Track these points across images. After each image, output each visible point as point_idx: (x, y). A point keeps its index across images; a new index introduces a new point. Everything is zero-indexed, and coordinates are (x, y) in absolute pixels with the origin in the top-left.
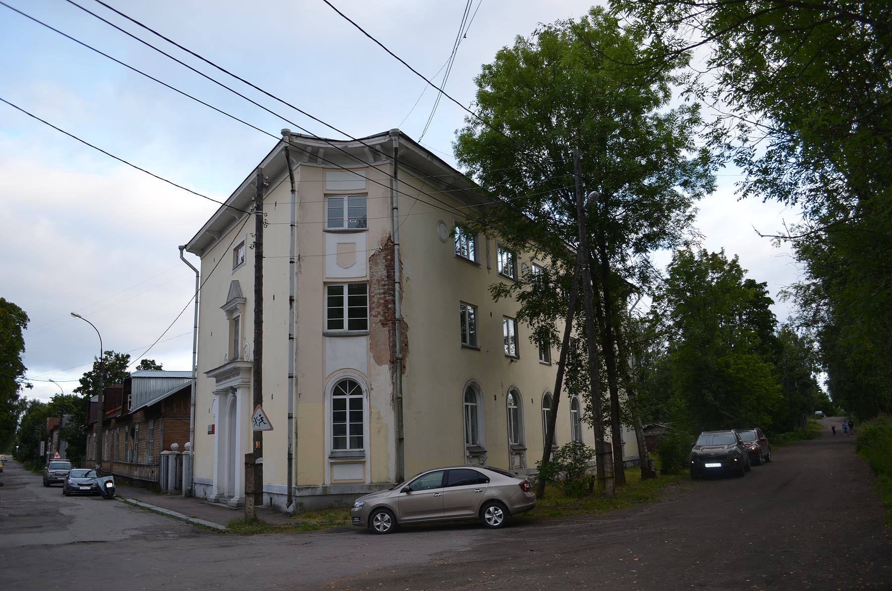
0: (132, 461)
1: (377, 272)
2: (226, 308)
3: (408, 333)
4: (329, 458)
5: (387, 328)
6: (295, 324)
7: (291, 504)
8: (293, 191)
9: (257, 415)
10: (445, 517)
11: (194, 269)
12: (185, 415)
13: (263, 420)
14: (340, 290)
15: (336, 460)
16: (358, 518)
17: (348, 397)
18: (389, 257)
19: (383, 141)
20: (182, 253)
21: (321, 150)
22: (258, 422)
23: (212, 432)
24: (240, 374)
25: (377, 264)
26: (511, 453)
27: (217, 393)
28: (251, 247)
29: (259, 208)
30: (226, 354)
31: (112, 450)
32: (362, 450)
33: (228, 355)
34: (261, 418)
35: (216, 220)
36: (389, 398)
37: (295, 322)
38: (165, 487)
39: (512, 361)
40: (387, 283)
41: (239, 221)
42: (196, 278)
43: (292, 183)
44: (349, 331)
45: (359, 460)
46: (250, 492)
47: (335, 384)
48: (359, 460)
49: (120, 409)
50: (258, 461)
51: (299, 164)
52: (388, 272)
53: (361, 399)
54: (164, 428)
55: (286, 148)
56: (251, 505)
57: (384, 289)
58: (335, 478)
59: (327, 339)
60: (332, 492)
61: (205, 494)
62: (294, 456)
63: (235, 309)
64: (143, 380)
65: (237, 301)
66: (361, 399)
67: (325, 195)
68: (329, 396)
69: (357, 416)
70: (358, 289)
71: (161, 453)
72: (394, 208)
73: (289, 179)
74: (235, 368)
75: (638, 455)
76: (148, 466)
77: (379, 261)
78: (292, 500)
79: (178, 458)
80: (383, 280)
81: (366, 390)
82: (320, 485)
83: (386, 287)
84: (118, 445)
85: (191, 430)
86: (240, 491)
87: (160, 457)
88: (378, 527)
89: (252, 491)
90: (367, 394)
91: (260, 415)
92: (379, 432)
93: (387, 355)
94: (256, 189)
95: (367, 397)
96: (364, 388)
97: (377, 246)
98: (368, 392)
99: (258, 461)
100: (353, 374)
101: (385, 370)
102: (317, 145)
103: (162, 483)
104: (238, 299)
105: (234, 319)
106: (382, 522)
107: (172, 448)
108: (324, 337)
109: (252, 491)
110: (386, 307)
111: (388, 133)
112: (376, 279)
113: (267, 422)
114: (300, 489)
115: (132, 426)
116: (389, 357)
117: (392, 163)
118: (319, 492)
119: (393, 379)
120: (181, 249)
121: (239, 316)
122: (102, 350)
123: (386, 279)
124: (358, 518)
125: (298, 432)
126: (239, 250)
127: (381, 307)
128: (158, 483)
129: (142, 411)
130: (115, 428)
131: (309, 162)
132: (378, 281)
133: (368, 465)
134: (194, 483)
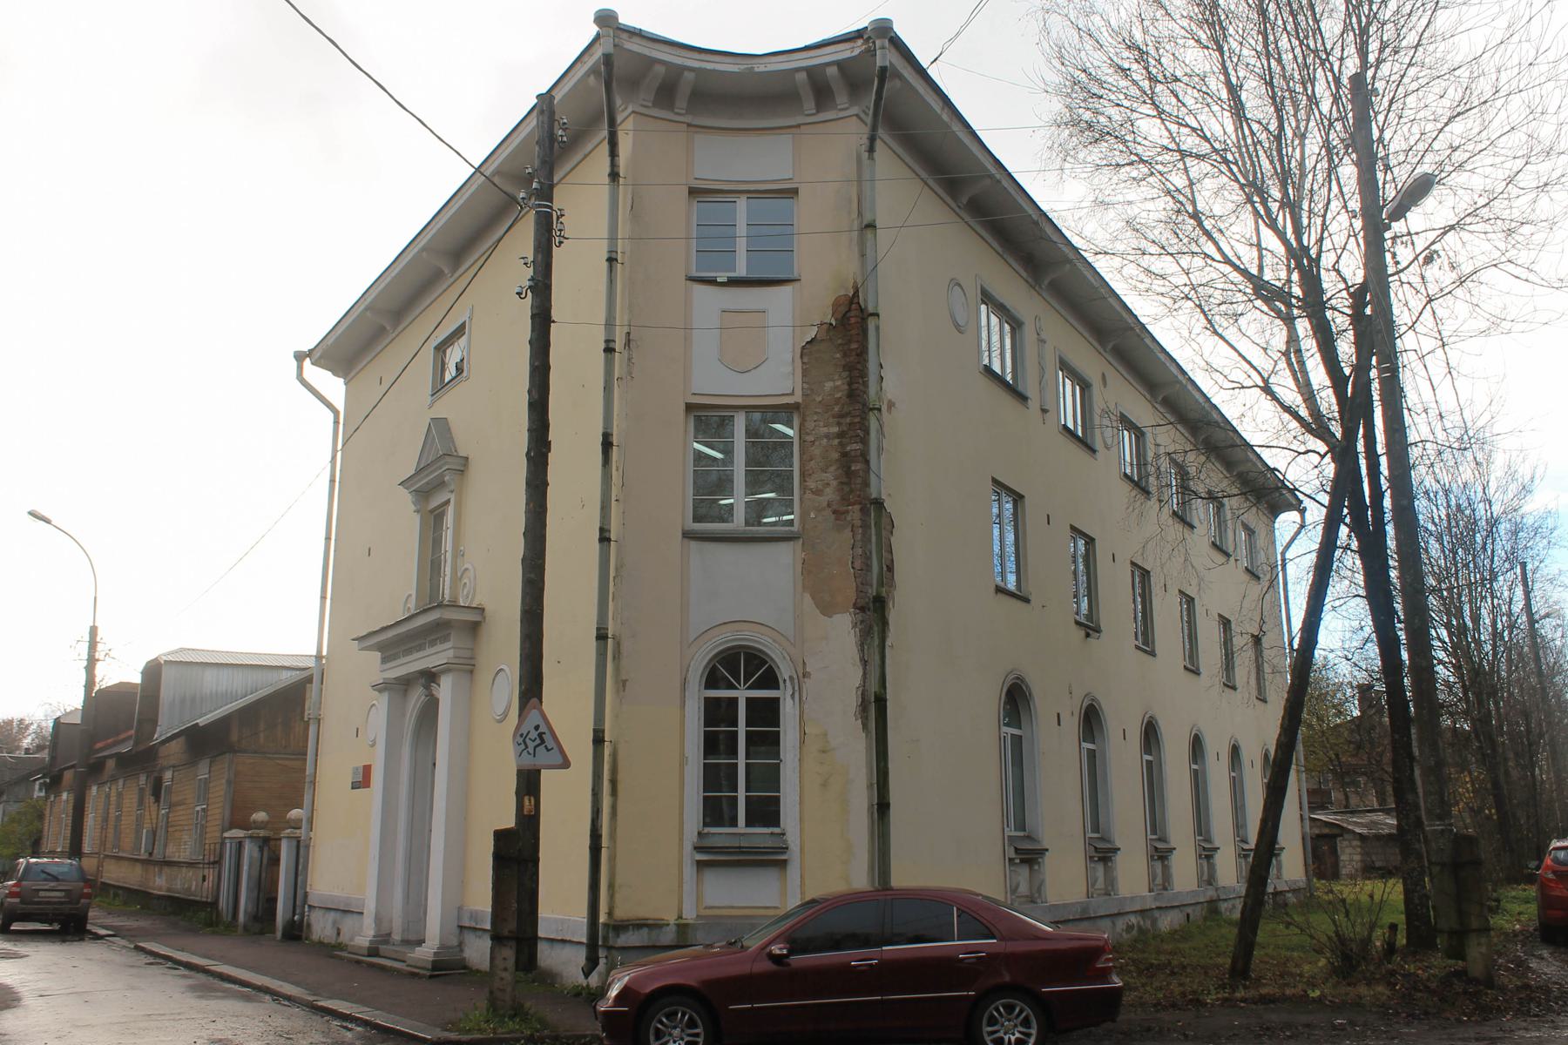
0: (151, 854)
2: (412, 485)
3: (892, 540)
4: (695, 848)
6: (613, 503)
7: (594, 969)
8: (614, 176)
9: (528, 726)
13: (543, 741)
15: (713, 859)
17: (742, 694)
18: (854, 346)
19: (847, 54)
20: (300, 368)
21: (686, 73)
22: (531, 745)
23: (363, 780)
26: (1090, 857)
27: (381, 688)
28: (519, 294)
29: (546, 193)
30: (410, 595)
31: (104, 829)
32: (776, 830)
33: (414, 596)
34: (540, 735)
36: (853, 701)
37: (613, 498)
39: (1088, 635)
41: (452, 280)
42: (332, 425)
43: (613, 153)
44: (747, 528)
45: (772, 859)
47: (711, 660)
48: (772, 859)
49: (129, 738)
51: (630, 110)
52: (850, 384)
53: (777, 700)
55: (607, 59)
56: (505, 969)
57: (839, 424)
58: (710, 902)
59: (694, 545)
61: (339, 934)
62: (605, 842)
63: (440, 484)
65: (446, 463)
66: (777, 700)
67: (693, 192)
68: (697, 689)
71: (226, 835)
73: (605, 147)
74: (438, 624)
75: (1304, 878)
76: (191, 865)
78: (598, 958)
79: (266, 849)
81: (791, 678)
82: (671, 918)
84: (118, 818)
85: (307, 780)
87: (223, 844)
89: (509, 932)
90: (793, 688)
91: (537, 728)
92: (824, 785)
93: (848, 591)
94: (537, 148)
95: (793, 696)
96: (784, 671)
98: (796, 681)
101: (842, 629)
102: (679, 61)
103: (224, 903)
104: (448, 459)
105: (432, 511)
107: (254, 822)
108: (686, 540)
109: (509, 932)
111: (859, 34)
112: (819, 399)
115: (156, 774)
116: (851, 594)
117: (862, 115)
120: (300, 357)
121: (448, 502)
125: (621, 776)
126: (448, 351)
128: (214, 904)
129: (182, 740)
130: (114, 779)
133: (793, 871)
134: (310, 906)
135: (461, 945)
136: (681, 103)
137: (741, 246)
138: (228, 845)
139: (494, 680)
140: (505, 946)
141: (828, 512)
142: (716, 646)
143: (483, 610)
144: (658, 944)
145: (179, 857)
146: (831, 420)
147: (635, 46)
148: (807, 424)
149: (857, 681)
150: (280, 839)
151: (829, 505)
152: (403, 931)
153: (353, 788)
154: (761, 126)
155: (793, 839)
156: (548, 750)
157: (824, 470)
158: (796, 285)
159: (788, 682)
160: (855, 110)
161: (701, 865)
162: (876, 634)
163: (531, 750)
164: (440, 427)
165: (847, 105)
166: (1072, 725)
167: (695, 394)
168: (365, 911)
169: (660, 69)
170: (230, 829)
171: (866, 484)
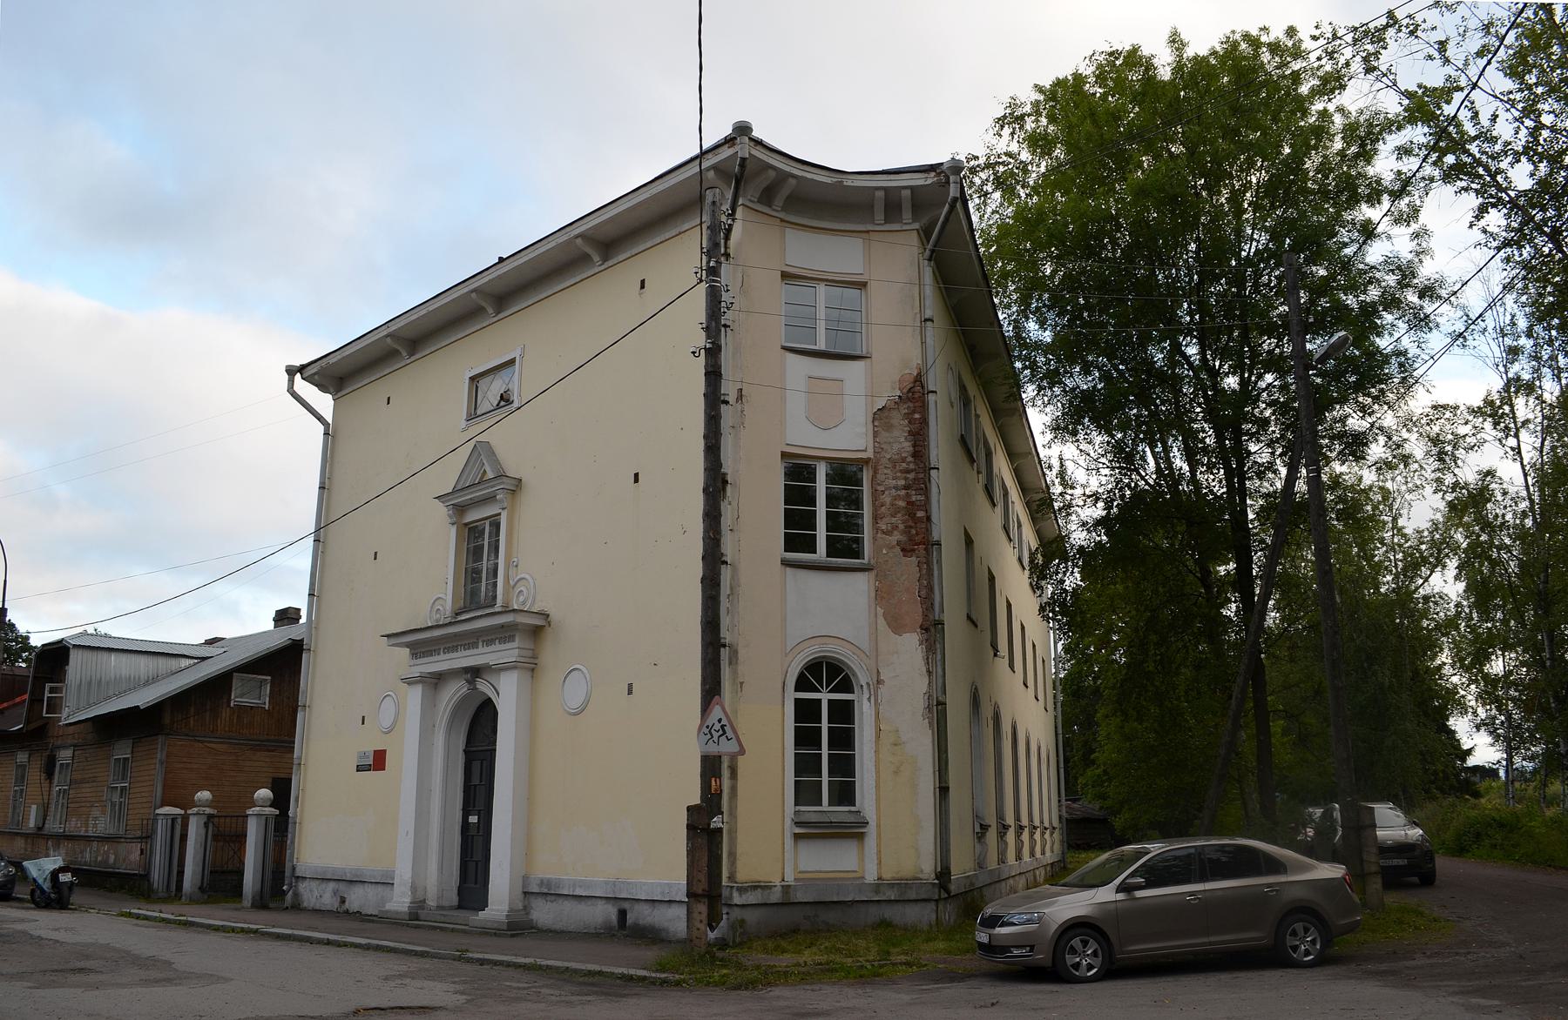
1: (890, 443)
5: (914, 558)
10: (1210, 943)
11: (320, 418)
12: (212, 732)
13: (724, 733)
14: (810, 474)
15: (810, 832)
16: (1028, 949)
18: (917, 416)
19: (921, 182)
20: (291, 382)
22: (716, 735)
24: (517, 639)
25: (889, 427)
28: (694, 353)
32: (853, 809)
34: (723, 727)
35: (429, 312)
36: (920, 703)
38: (165, 887)
40: (912, 466)
45: (853, 831)
46: (700, 892)
48: (853, 831)
50: (716, 822)
52: (914, 446)
53: (850, 703)
54: (167, 756)
56: (701, 921)
57: (906, 479)
60: (801, 897)
64: (95, 653)
65: (503, 483)
66: (850, 703)
67: (785, 276)
69: (844, 739)
70: (845, 474)
71: (158, 811)
72: (926, 320)
77: (895, 422)
80: (904, 460)
81: (868, 684)
83: (911, 476)
85: (296, 762)
86: (510, 893)
87: (155, 820)
88: (1077, 966)
89: (703, 890)
91: (720, 721)
93: (915, 613)
95: (869, 699)
96: (862, 677)
97: (888, 393)
99: (716, 822)
100: (830, 647)
101: (910, 646)
104: (505, 479)
105: (466, 524)
106: (1086, 958)
110: (912, 515)
112: (888, 457)
113: (733, 736)
114: (741, 890)
118: (775, 896)
119: (928, 663)
120: (291, 371)
122: (5, 581)
123: (910, 459)
124: (1028, 949)
127: (899, 515)
128: (146, 877)
129: (90, 724)
131: (758, 202)
132: (893, 462)
133: (871, 842)
135: (526, 908)
136: (779, 202)
137: (821, 327)
138: (160, 822)
139: (564, 681)
140: (700, 902)
141: (898, 549)
142: (813, 653)
143: (548, 616)
144: (768, 902)
145: (87, 831)
146: (899, 474)
147: (759, 153)
148: (878, 476)
149: (925, 688)
150: (247, 816)
151: (898, 544)
152: (438, 898)
153: (358, 771)
154: (809, 224)
155: (869, 812)
156: (729, 740)
157: (893, 516)
158: (868, 360)
159: (865, 687)
160: (916, 226)
161: (797, 837)
162: (939, 650)
163: (715, 739)
164: (482, 451)
165: (910, 221)
166: (896, 748)
167: (788, 444)
168: (396, 882)
169: (772, 174)
170: (162, 805)
171: (928, 531)
